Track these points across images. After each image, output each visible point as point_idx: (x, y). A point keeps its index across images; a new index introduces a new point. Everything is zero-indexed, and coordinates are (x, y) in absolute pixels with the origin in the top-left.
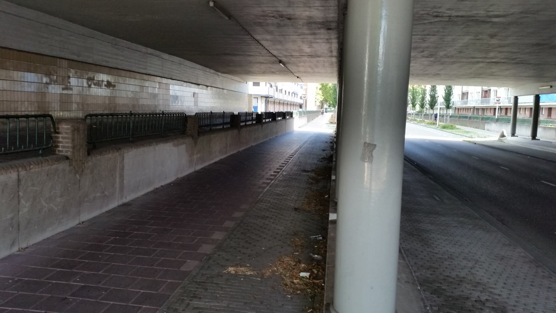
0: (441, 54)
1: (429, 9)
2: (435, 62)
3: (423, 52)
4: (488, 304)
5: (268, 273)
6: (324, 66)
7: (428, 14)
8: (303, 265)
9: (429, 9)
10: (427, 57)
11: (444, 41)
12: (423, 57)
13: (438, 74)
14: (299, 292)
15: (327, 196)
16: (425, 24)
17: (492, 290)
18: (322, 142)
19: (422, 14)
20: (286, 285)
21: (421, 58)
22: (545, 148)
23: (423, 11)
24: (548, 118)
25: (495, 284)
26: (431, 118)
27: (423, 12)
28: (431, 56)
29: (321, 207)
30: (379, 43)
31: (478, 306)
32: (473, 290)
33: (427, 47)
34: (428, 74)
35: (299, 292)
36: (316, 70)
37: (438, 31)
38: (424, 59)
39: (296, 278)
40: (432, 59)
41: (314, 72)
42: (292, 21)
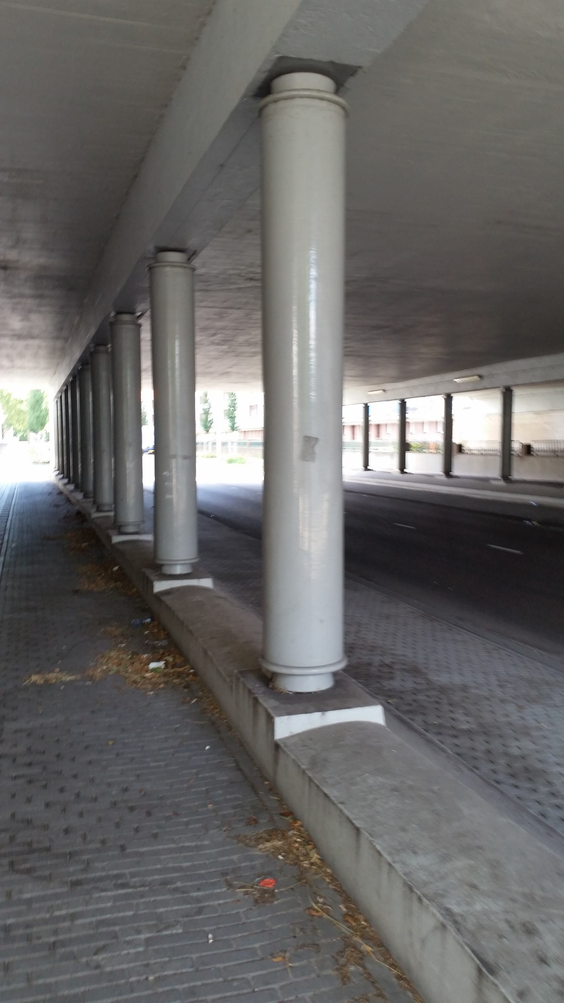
0: (241, 339)
1: (242, 268)
2: (227, 352)
3: (214, 335)
4: (396, 666)
5: (98, 673)
6: (35, 355)
7: (239, 275)
8: (145, 656)
9: (242, 268)
10: (218, 344)
11: (250, 319)
12: (213, 343)
13: (227, 373)
14: (162, 686)
15: (116, 568)
16: (230, 290)
17: (393, 652)
18: (50, 494)
19: (231, 275)
20: (135, 682)
21: (208, 345)
22: (385, 481)
23: (234, 269)
24: (378, 439)
25: (393, 645)
26: (207, 449)
27: (231, 272)
28: (225, 342)
29: (118, 583)
30: (309, 320)
31: (386, 670)
32: (372, 655)
33: (224, 328)
34: (211, 373)
35: (162, 686)
36: (18, 362)
37: (246, 303)
38: (212, 347)
39: (147, 671)
40: (224, 347)
41: (13, 367)
42: (8, 272)
